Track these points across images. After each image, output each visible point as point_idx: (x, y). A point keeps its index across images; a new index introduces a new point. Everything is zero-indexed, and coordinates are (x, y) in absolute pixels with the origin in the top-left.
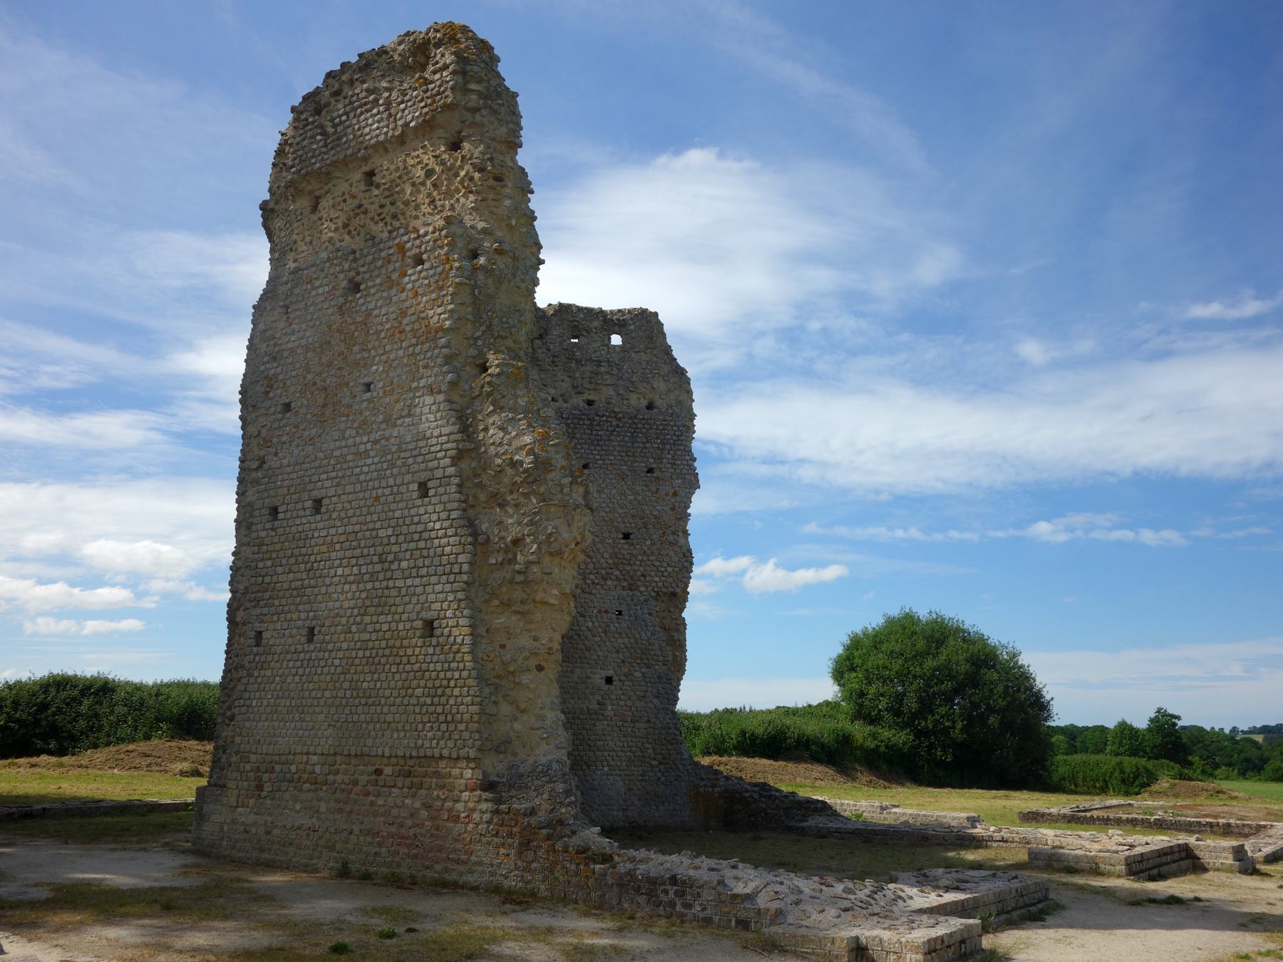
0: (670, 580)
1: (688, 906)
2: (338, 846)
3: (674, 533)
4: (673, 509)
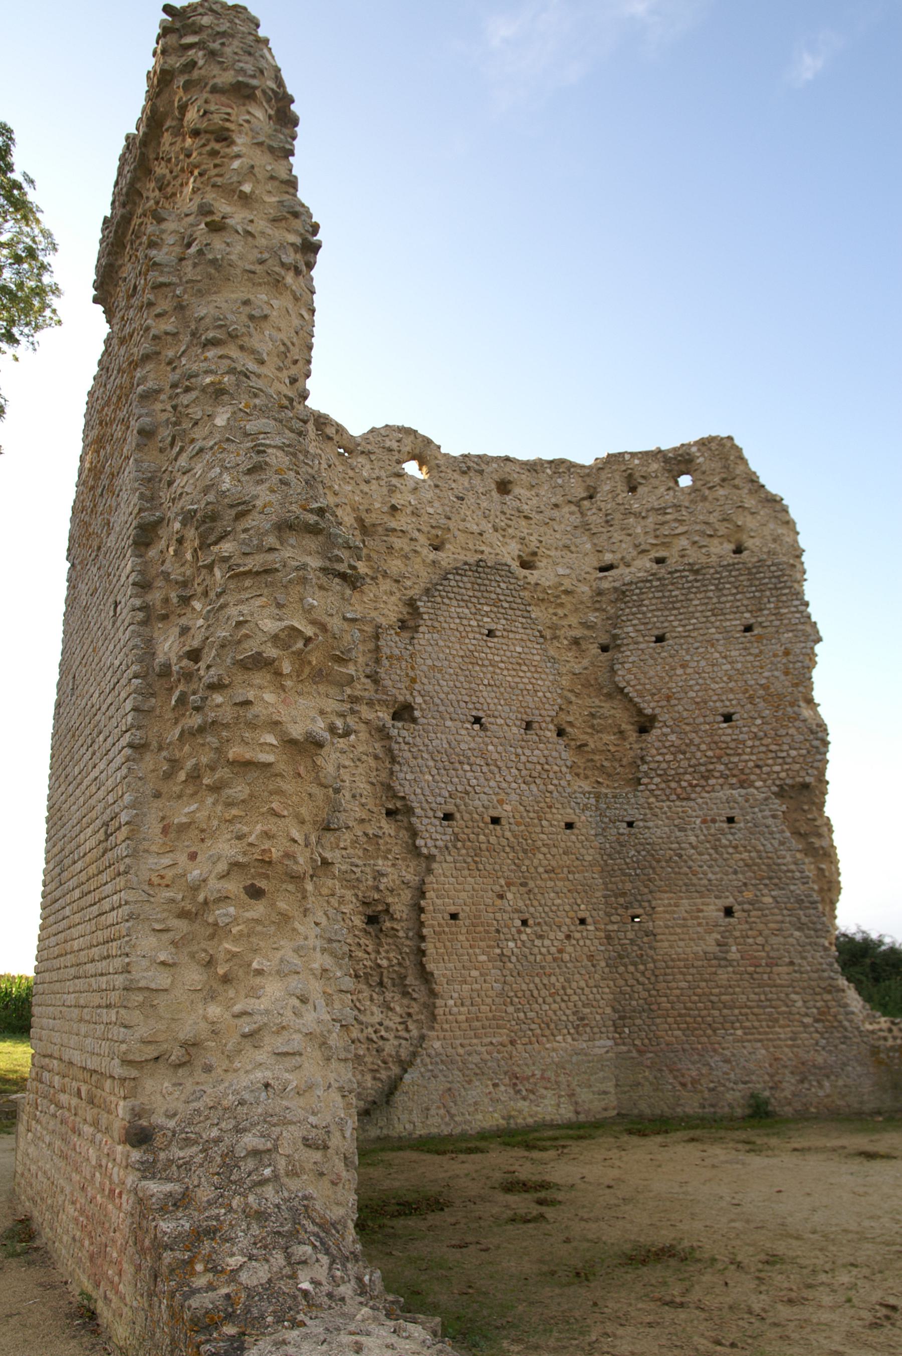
0: (797, 767)
3: (792, 704)
4: (786, 673)
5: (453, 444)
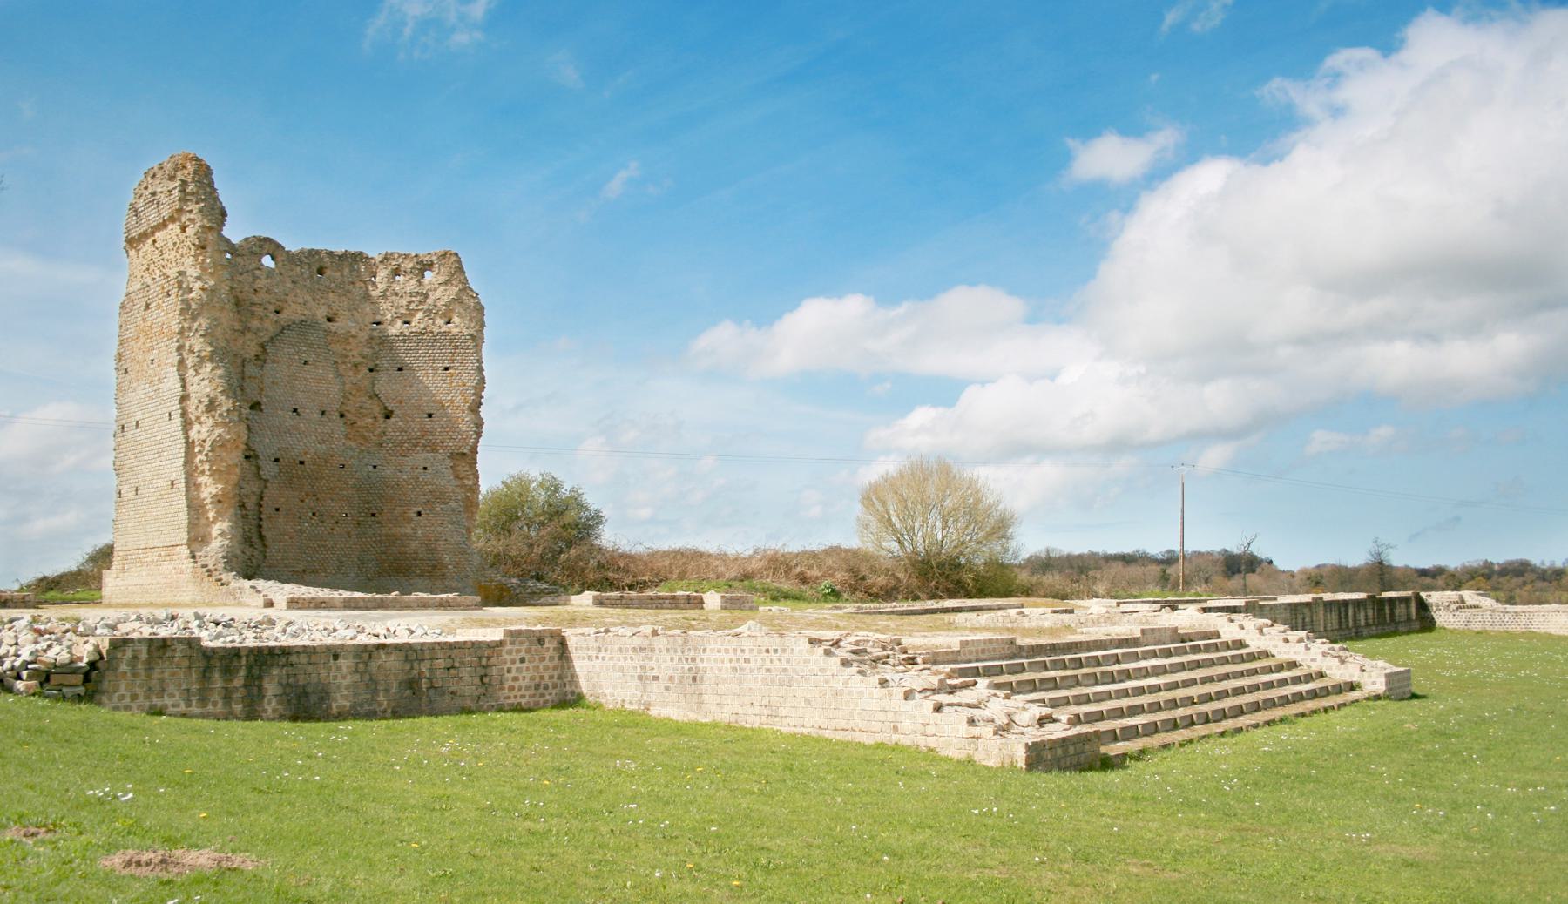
5: (292, 246)
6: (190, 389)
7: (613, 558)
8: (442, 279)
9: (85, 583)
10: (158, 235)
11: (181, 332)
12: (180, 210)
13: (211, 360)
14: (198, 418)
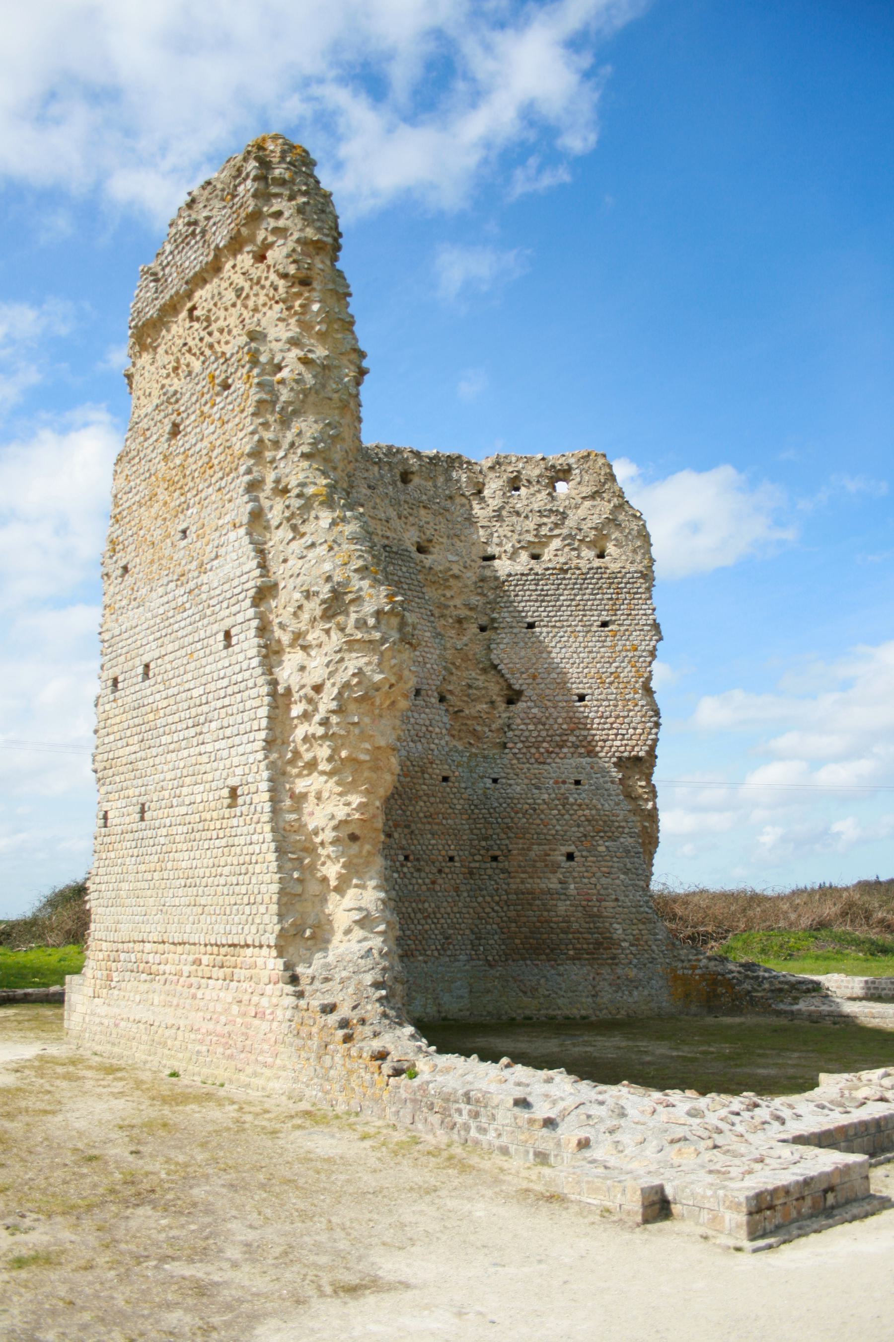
1: (483, 1130)
2: (169, 1042)
6: (278, 571)
7: (666, 904)
8: (587, 490)
9: (41, 937)
10: (202, 295)
11: (256, 453)
12: (255, 217)
13: (329, 503)
14: (298, 636)
